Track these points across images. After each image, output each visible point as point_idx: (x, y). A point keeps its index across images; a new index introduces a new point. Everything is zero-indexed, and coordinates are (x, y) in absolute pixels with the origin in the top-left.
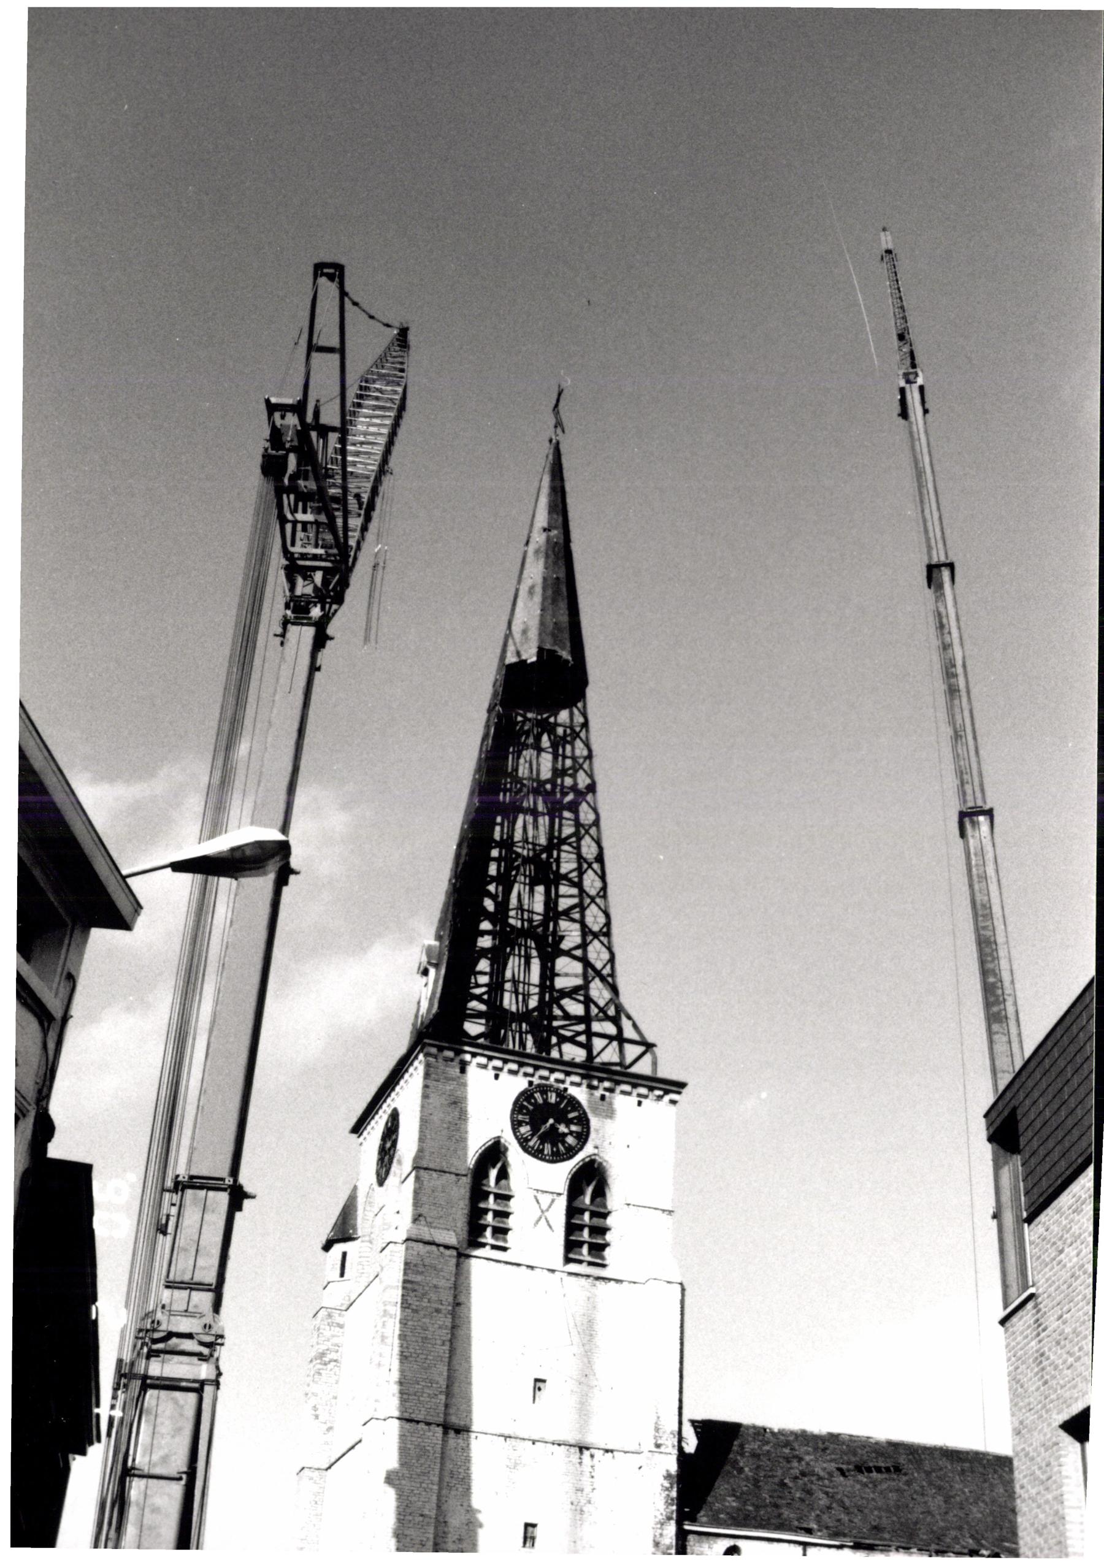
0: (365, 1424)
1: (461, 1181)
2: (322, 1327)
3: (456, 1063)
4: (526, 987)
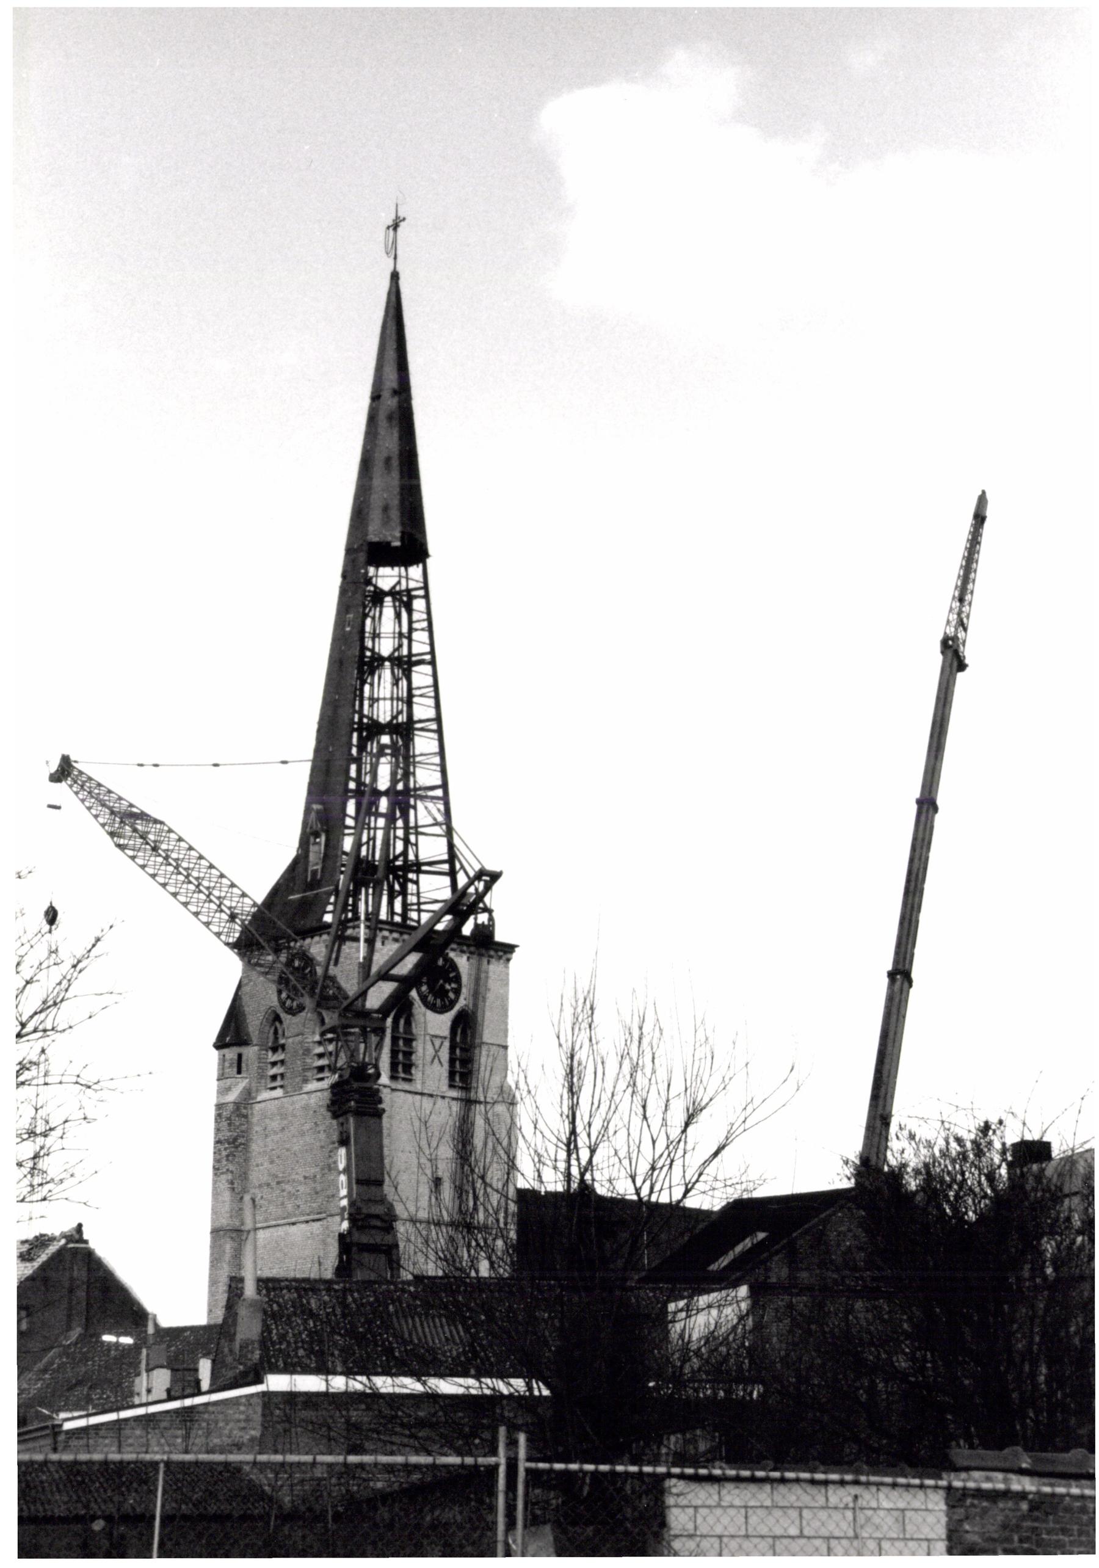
2: (233, 1118)
4: (415, 907)
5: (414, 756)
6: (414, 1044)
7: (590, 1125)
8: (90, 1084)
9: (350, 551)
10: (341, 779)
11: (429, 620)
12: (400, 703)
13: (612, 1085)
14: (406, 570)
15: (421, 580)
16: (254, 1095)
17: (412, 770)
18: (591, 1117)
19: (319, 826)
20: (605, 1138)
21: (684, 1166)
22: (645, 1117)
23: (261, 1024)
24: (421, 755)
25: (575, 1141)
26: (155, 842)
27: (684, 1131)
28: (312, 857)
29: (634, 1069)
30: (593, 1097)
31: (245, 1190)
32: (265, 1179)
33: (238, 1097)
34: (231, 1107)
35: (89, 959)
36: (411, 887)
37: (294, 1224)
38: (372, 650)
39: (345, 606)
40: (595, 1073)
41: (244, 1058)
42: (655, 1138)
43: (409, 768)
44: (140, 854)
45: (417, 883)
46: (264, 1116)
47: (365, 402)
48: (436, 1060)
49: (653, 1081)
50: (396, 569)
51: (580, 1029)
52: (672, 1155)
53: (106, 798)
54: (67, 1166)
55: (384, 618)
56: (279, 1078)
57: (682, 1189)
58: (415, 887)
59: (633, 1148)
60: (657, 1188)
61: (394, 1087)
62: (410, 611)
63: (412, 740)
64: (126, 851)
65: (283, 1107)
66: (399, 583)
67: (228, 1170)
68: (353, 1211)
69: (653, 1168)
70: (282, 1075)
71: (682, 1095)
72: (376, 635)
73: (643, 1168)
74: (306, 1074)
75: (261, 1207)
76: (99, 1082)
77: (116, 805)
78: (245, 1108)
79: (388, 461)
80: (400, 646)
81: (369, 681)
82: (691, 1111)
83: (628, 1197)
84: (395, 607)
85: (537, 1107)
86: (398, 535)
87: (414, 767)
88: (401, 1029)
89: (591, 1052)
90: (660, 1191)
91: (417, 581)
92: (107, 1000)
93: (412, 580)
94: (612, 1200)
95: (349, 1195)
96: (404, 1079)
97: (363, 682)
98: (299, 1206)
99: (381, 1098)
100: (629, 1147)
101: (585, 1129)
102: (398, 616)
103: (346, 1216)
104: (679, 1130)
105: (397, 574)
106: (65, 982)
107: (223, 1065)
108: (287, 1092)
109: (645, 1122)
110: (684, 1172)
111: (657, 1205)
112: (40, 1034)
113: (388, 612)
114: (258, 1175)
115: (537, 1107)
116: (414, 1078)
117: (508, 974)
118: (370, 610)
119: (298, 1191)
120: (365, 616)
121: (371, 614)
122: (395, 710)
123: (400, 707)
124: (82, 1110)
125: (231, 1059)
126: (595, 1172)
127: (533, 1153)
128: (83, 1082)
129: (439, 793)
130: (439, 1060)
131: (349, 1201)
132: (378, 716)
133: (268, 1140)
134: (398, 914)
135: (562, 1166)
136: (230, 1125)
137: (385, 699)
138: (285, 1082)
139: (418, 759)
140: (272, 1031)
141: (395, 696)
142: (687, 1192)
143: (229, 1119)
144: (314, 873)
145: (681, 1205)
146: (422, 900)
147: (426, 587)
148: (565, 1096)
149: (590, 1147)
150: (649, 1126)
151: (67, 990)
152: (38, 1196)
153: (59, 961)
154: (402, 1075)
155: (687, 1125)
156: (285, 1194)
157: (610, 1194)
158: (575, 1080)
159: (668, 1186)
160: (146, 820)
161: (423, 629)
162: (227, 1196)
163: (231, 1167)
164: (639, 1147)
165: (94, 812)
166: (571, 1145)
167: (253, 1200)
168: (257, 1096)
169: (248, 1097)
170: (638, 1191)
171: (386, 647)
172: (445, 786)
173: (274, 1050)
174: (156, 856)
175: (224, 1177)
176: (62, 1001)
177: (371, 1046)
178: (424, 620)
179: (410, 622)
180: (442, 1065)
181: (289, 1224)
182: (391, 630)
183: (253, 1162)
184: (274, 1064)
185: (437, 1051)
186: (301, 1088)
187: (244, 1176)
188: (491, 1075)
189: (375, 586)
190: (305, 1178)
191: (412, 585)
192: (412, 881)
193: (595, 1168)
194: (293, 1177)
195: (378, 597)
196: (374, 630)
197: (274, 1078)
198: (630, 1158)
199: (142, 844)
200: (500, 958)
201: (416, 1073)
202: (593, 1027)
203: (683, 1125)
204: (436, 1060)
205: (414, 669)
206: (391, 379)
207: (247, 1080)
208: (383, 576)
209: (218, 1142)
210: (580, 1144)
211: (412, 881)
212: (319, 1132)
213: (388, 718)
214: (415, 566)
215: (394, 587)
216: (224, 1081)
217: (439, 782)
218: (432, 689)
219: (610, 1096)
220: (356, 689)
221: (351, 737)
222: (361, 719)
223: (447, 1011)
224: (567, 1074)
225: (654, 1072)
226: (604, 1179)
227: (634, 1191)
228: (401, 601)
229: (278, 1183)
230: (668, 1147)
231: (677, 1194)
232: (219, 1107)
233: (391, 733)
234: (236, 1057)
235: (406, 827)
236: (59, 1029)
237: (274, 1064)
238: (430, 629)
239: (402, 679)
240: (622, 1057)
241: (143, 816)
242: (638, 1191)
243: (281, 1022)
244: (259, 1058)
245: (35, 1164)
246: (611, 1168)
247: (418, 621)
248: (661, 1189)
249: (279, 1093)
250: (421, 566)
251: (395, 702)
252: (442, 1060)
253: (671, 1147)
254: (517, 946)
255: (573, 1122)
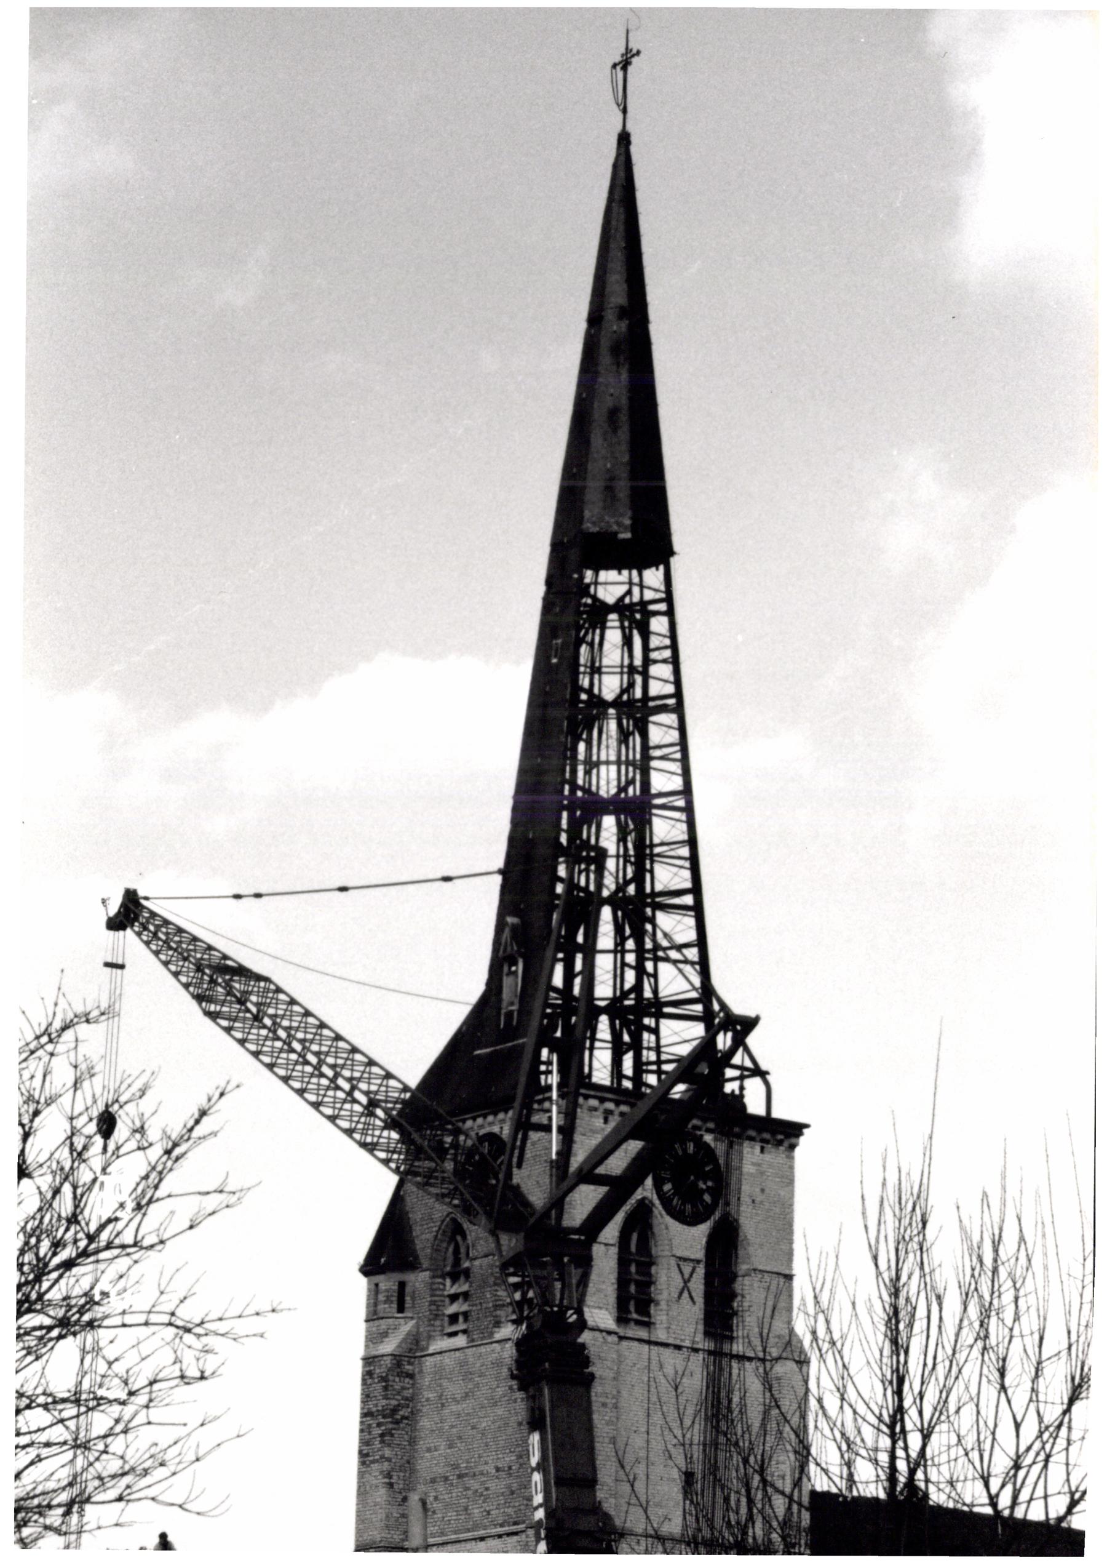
0: (941, 1227)
1: (610, 1252)
2: (391, 1378)
3: (599, 1113)
4: (654, 1067)
5: (652, 846)
6: (653, 1270)
7: (921, 1396)
8: (190, 1326)
9: (557, 547)
10: (545, 878)
11: (674, 647)
12: (631, 769)
13: (952, 1339)
14: (640, 575)
15: (663, 588)
16: (424, 1343)
17: (648, 866)
18: (922, 1383)
19: (515, 948)
20: (943, 1418)
21: (1067, 1464)
22: (1003, 1388)
23: (436, 1237)
24: (662, 844)
25: (902, 1420)
26: (258, 1005)
27: (1067, 1411)
28: (506, 994)
29: (986, 1313)
30: (925, 1355)
31: (409, 1487)
32: (440, 1470)
33: (399, 1346)
34: (388, 1361)
35: (191, 1142)
36: (648, 1038)
37: (482, 1539)
38: (589, 691)
39: (549, 630)
40: (929, 1317)
41: (408, 1289)
42: (1019, 1419)
43: (644, 864)
44: (237, 1025)
45: (656, 1031)
46: (439, 1372)
47: (581, 326)
48: (686, 1294)
49: (1016, 1332)
50: (625, 573)
51: (906, 1252)
52: (1048, 1447)
53: (191, 947)
54: (153, 1450)
55: (607, 646)
56: (461, 1319)
57: (1065, 1500)
58: (653, 1038)
59: (986, 1434)
60: (1024, 1496)
61: (622, 1334)
62: (646, 635)
63: (650, 823)
64: (219, 1021)
65: (466, 1363)
66: (629, 592)
67: (382, 1457)
68: (553, 1524)
69: (1017, 1466)
70: (466, 1315)
71: (1064, 1354)
72: (596, 670)
73: (1001, 1464)
74: (498, 1312)
75: (434, 1512)
76: (202, 1323)
77: (206, 957)
78: (409, 1363)
79: (613, 413)
80: (631, 685)
81: (584, 736)
82: (1077, 1381)
83: (976, 1509)
84: (622, 628)
85: (844, 1366)
86: (628, 522)
87: (652, 862)
88: (633, 1248)
89: (922, 1285)
90: (1029, 1502)
91: (656, 590)
92: (213, 1201)
93: (649, 588)
94: (955, 1512)
95: (546, 1504)
96: (638, 1323)
97: (577, 738)
98: (488, 1513)
99: (588, 1358)
100: (979, 1434)
101: (915, 1402)
102: (628, 642)
103: (543, 1533)
104: (1059, 1409)
105: (627, 580)
106: (154, 1175)
107: (376, 1299)
108: (473, 1340)
109: (1003, 1395)
110: (1068, 1474)
111: (1025, 1523)
112: (116, 1252)
113: (613, 636)
114: (429, 1464)
115: (844, 1366)
116: (653, 1320)
117: (792, 1168)
118: (586, 633)
119: (487, 1489)
120: (580, 642)
121: (589, 638)
122: (623, 779)
123: (631, 775)
124: (178, 1366)
125: (387, 1291)
126: (929, 1469)
127: (838, 1436)
128: (179, 1323)
129: (688, 900)
130: (690, 1293)
131: (546, 1511)
132: (598, 787)
133: (446, 1411)
134: (627, 1078)
135: (884, 1458)
136: (386, 1388)
137: (608, 763)
138: (470, 1326)
139: (657, 850)
140: (451, 1249)
141: (623, 758)
142: (1073, 1504)
143: (384, 1379)
144: (509, 1015)
145: (1064, 1525)
146: (664, 1057)
147: (669, 599)
148: (887, 1351)
149: (921, 1431)
150: (1009, 1401)
151: (156, 1187)
152: (112, 1494)
153: (146, 1144)
154: (635, 1316)
155: (1072, 1401)
156: (470, 1493)
157: (951, 1505)
158: (901, 1326)
159: (1042, 1494)
160: (246, 976)
161: (664, 661)
162: (381, 1495)
163: (387, 1452)
164: (993, 1433)
165: (173, 968)
166: (895, 1425)
167: (424, 1503)
168: (428, 1345)
169: (414, 1349)
170: (993, 1501)
171: (610, 686)
172: (696, 889)
173: (455, 1277)
174: (259, 1028)
175: (375, 1466)
176: (150, 1202)
177: (570, 1285)
178: (666, 647)
179: (646, 649)
180: (694, 1302)
181: (475, 1539)
182: (618, 662)
183: (422, 1445)
184: (454, 1298)
185: (686, 1282)
186: (491, 1334)
187: (408, 1466)
188: (772, 1317)
189: (594, 598)
190: (498, 1469)
191: (649, 595)
192: (649, 1029)
193: (929, 1463)
194: (481, 1468)
195: (599, 612)
196: (593, 662)
197: (454, 1319)
198: (980, 1450)
199: (240, 1011)
200: (780, 1143)
201: (659, 1315)
202: (925, 1249)
203: (1066, 1401)
204: (686, 1294)
205: (652, 719)
206: (618, 296)
207: (414, 1322)
208: (606, 583)
209: (366, 1414)
210: (909, 1426)
211: (649, 1029)
212: (515, 1401)
213: (613, 791)
214: (654, 569)
215: (622, 598)
216: (377, 1323)
217: (688, 885)
218: (678, 748)
219: (950, 1352)
220: (566, 749)
221: (559, 818)
222: (573, 791)
223: (702, 1221)
224: (890, 1319)
225: (1017, 1318)
226: (942, 1479)
227: (986, 1501)
228: (632, 621)
229: (460, 1476)
230: (1041, 1434)
231: (1058, 1507)
232: (369, 1361)
233: (616, 813)
234: (396, 1288)
235: (640, 951)
236: (146, 1243)
237: (454, 1298)
238: (675, 661)
239: (633, 733)
240: (967, 1294)
241: (241, 971)
242: (993, 1501)
243: (464, 1238)
244: (432, 1290)
245: (106, 1446)
246: (952, 1463)
247: (657, 649)
248: (1031, 1499)
249: (461, 1341)
250: (661, 567)
251: (623, 768)
252: (694, 1294)
253: (1046, 1436)
254: (807, 1126)
255: (899, 1393)
